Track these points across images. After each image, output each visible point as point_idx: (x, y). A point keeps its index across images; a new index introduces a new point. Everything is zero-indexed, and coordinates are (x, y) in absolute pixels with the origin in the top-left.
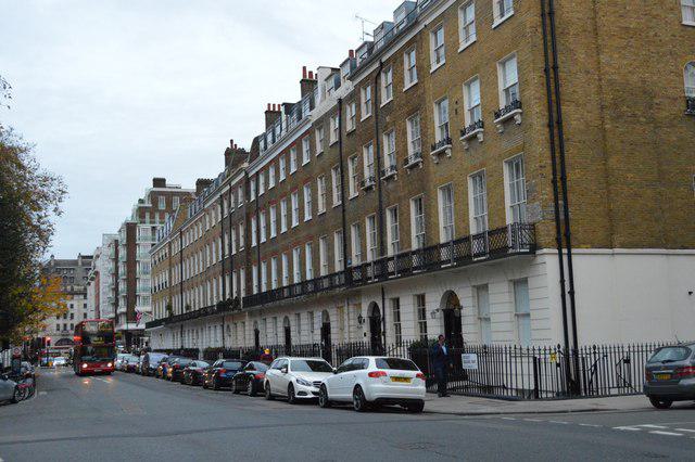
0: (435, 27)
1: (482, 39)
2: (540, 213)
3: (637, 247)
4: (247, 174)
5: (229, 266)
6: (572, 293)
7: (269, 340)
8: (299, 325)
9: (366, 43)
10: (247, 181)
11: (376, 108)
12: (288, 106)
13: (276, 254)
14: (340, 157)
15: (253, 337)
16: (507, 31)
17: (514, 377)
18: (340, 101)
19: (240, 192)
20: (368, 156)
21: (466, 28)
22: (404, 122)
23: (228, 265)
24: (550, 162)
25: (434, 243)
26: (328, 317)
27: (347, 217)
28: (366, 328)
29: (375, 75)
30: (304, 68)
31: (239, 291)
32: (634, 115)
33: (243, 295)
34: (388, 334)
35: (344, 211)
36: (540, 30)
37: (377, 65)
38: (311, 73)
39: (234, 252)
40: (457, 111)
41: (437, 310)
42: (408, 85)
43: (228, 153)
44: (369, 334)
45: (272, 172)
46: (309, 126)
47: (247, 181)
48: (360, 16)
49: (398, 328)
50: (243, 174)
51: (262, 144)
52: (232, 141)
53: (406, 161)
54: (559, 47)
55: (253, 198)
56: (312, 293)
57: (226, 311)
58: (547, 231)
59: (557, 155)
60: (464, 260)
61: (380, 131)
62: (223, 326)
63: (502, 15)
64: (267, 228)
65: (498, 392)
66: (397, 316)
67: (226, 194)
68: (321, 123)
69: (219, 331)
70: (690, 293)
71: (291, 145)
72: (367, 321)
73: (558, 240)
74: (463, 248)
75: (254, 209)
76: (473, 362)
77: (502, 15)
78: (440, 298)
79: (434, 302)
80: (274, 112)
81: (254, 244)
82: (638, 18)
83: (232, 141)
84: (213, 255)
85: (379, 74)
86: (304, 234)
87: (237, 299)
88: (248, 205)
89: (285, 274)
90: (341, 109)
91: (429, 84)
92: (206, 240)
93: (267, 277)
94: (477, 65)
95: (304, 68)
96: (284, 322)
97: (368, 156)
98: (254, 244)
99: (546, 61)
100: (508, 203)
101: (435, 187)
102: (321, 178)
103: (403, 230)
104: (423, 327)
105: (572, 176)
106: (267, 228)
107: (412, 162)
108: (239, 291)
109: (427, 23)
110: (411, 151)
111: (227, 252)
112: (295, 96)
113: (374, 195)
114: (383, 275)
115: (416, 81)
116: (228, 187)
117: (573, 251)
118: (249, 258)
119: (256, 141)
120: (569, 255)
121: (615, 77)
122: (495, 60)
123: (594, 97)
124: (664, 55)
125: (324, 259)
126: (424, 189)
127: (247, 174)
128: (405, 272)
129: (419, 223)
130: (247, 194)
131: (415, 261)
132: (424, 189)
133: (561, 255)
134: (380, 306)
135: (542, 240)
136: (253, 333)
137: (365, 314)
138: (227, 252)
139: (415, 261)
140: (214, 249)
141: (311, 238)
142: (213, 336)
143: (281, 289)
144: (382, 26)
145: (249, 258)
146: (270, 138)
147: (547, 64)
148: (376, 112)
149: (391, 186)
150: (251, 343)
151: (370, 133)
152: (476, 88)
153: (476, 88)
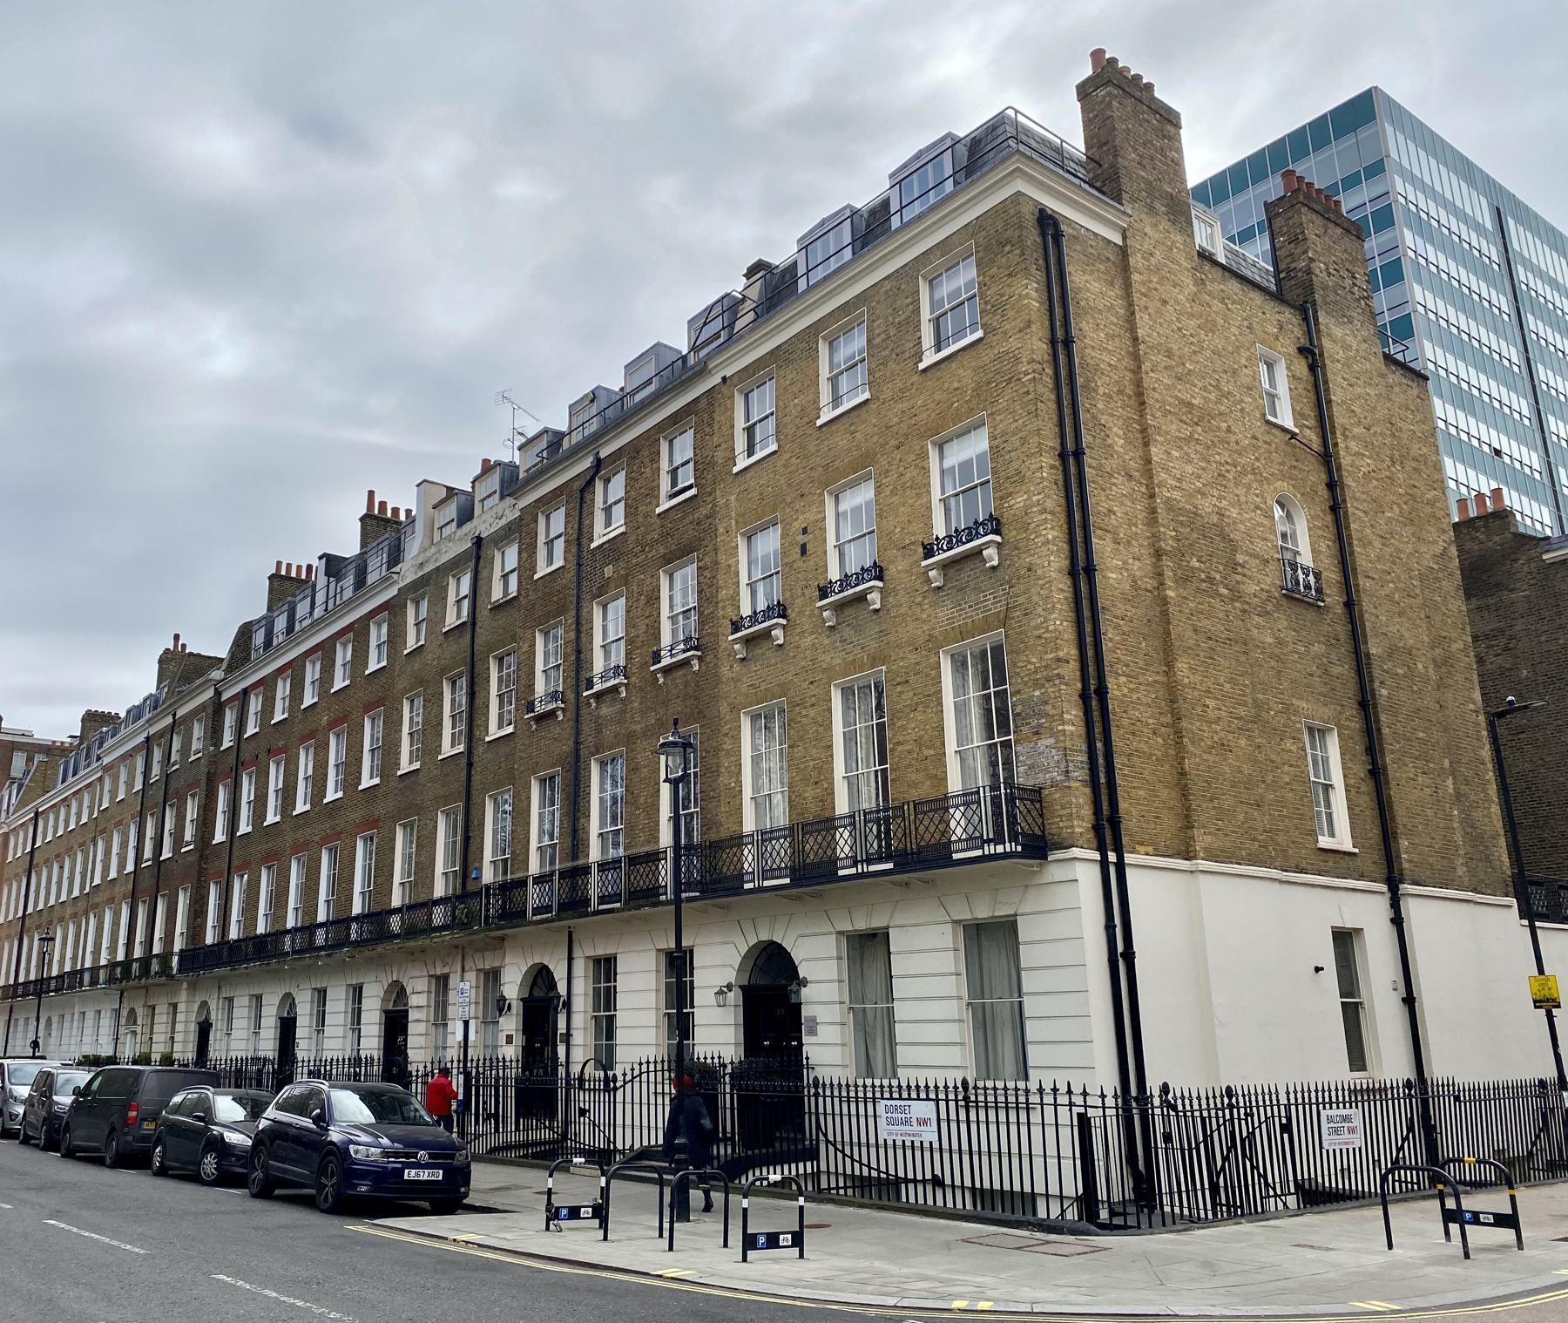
0: (752, 376)
1: (887, 395)
2: (1052, 758)
3: (1229, 859)
4: (218, 693)
5: (149, 884)
6: (1129, 956)
7: (234, 1045)
8: (230, 1020)
9: (546, 431)
10: (217, 708)
11: (580, 551)
12: (333, 565)
13: (276, 859)
14: (468, 654)
15: (193, 1038)
16: (964, 375)
17: (1026, 1161)
18: (478, 541)
19: (198, 731)
20: (545, 654)
21: (550, 543)
22: (821, 494)
23: (147, 882)
24: (1074, 652)
25: (724, 834)
26: (293, 1005)
27: (476, 778)
28: (511, 1024)
29: (577, 485)
30: (371, 493)
31: (168, 939)
32: (1211, 580)
33: (178, 945)
34: (578, 1038)
35: (470, 765)
36: (1049, 371)
37: (587, 463)
38: (383, 505)
39: (166, 854)
40: (804, 547)
41: (729, 987)
42: (373, 666)
43: (166, 659)
44: (519, 1040)
45: (283, 689)
46: (393, 591)
47: (217, 708)
48: (512, 395)
49: (606, 1028)
50: (210, 693)
51: (259, 638)
52: (177, 637)
53: (657, 657)
54: (1083, 416)
55: (227, 742)
56: (368, 937)
57: (132, 979)
58: (1074, 810)
59: (1088, 640)
60: (575, 905)
61: (587, 597)
62: (118, 1012)
63: (750, 451)
64: (257, 803)
65: (909, 1194)
66: (606, 999)
67: (161, 734)
68: (430, 585)
69: (106, 1022)
70: (1318, 969)
71: (280, 671)
72: (517, 1008)
73: (1097, 828)
74: (420, 915)
75: (226, 768)
76: (923, 1122)
77: (750, 451)
78: (744, 949)
79: (719, 964)
80: (288, 578)
81: (219, 837)
82: (1204, 389)
83: (177, 637)
84: (116, 858)
85: (591, 482)
86: (356, 816)
87: (512, 888)
88: (215, 758)
89: (139, 936)
90: (478, 558)
91: (729, 500)
92: (98, 828)
93: (241, 909)
94: (879, 448)
95: (371, 493)
96: (199, 1013)
97: (545, 654)
98: (219, 837)
99: (1062, 436)
100: (951, 745)
101: (735, 709)
102: (193, 796)
103: (342, 883)
104: (681, 1025)
105: (1117, 686)
106: (257, 803)
107: (539, 709)
108: (168, 939)
109: (728, 372)
110: (540, 688)
111: (148, 854)
112: (348, 545)
113: (561, 729)
114: (575, 905)
115: (384, 663)
116: (169, 720)
117: (1129, 858)
118: (206, 866)
119: (245, 632)
120: (1121, 867)
121: (1176, 495)
122: (924, 436)
123: (1140, 528)
124: (1244, 473)
125: (419, 864)
126: (699, 715)
127: (218, 693)
128: (644, 896)
129: (407, 858)
130: (215, 733)
131: (438, 916)
132: (699, 715)
133: (1104, 864)
134: (560, 974)
135: (1057, 825)
136: (193, 1027)
137: (512, 987)
138: (148, 854)
139: (438, 916)
140: (115, 849)
141: (373, 823)
142: (88, 1031)
143: (277, 935)
144: (593, 397)
145: (206, 866)
146: (281, 623)
147: (1063, 444)
148: (579, 557)
149: (605, 710)
150: (111, 1053)
151: (562, 603)
152: (618, 607)
153: (618, 607)
